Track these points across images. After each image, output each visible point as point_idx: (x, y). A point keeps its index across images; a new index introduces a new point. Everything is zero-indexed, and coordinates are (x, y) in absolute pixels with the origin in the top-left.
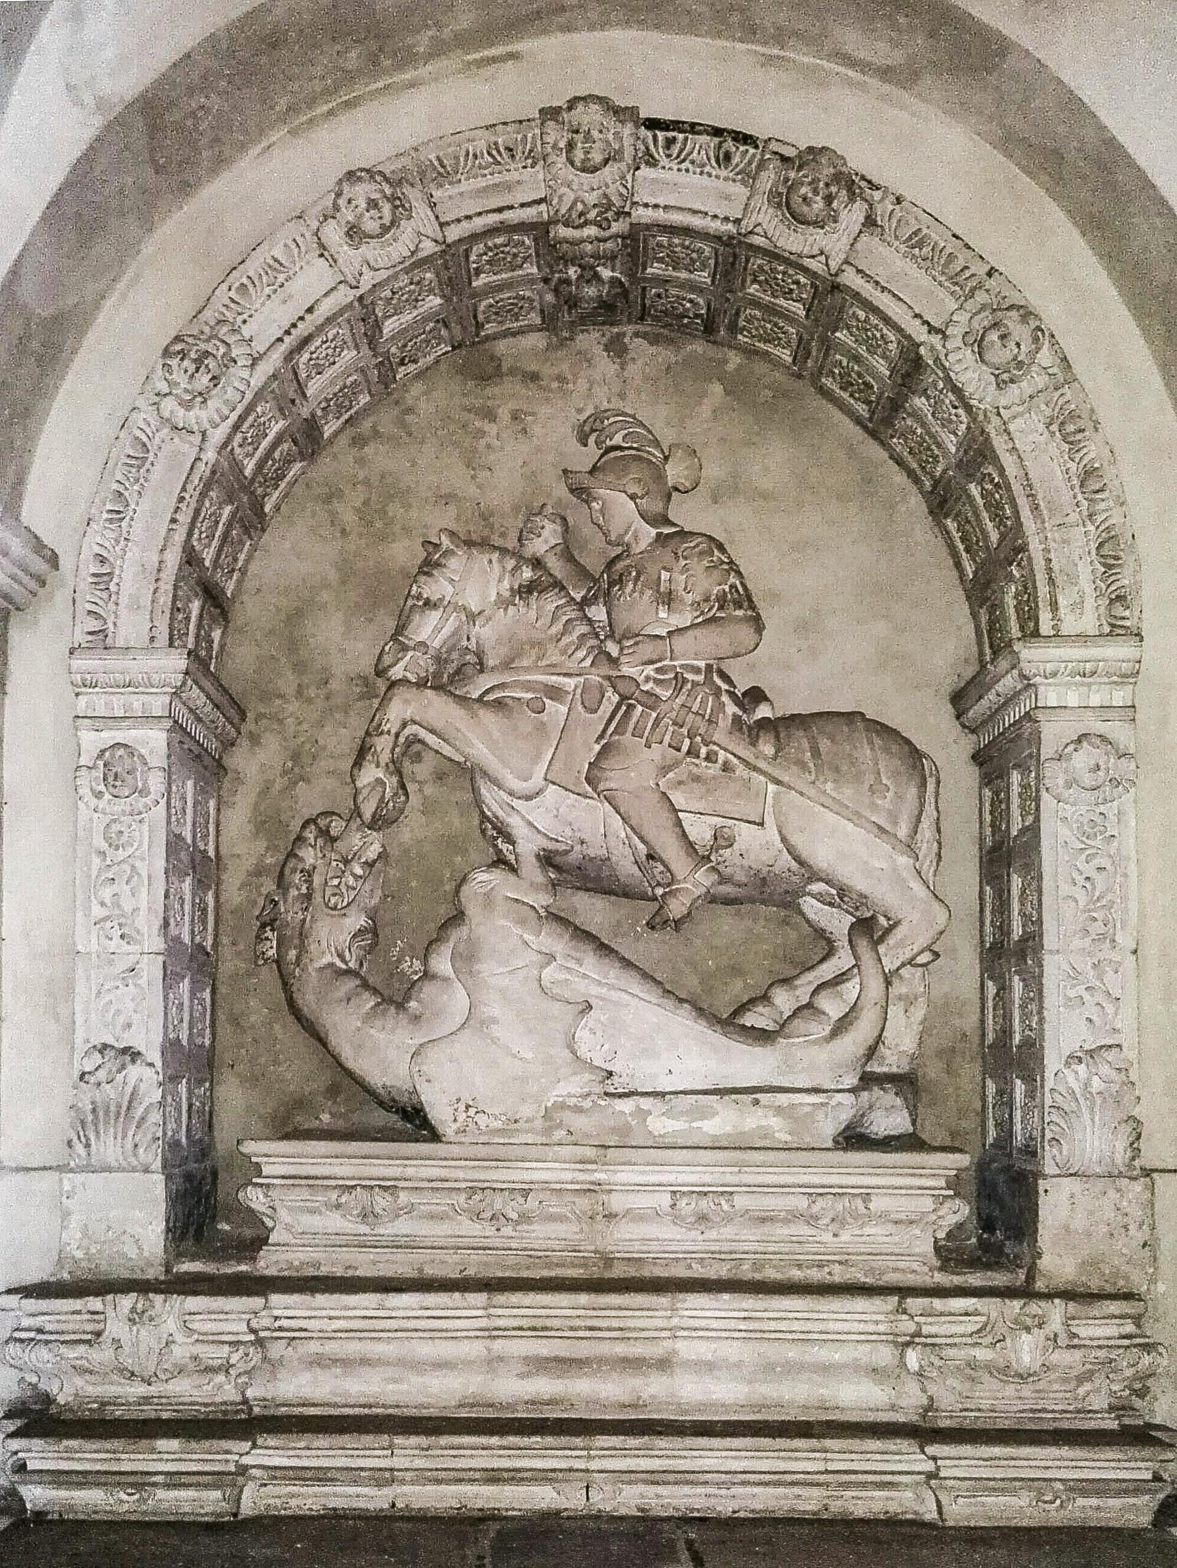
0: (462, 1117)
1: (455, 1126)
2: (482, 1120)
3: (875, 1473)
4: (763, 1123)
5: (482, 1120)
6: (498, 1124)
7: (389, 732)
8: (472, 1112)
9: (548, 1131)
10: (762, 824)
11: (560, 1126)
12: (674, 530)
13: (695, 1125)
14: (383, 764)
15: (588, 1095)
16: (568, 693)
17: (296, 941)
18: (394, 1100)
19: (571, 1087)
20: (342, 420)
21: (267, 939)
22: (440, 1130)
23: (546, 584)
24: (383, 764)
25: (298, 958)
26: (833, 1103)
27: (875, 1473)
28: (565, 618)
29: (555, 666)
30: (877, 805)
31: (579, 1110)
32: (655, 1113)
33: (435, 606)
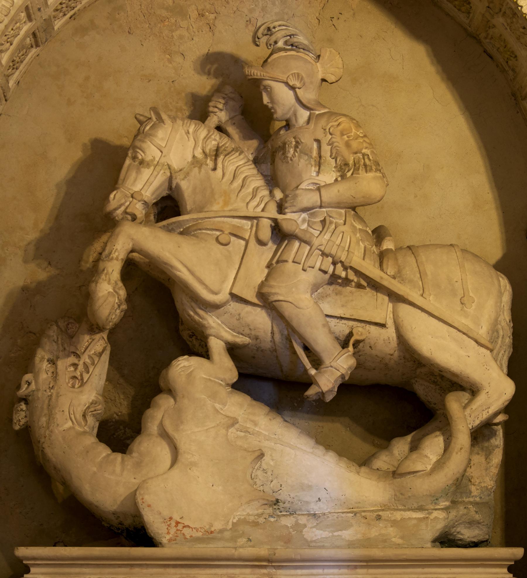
0: (173, 530)
1: (168, 537)
2: (186, 531)
3: (430, 573)
4: (383, 532)
5: (186, 531)
6: (200, 534)
7: (117, 259)
8: (180, 527)
9: (234, 539)
10: (383, 326)
11: (241, 536)
12: (326, 110)
13: (336, 534)
14: (112, 282)
15: (262, 514)
16: (246, 230)
17: (46, 411)
18: (121, 523)
19: (250, 511)
20: (69, 15)
21: (22, 410)
22: (157, 538)
23: (229, 149)
24: (112, 282)
25: (48, 423)
26: (432, 516)
27: (430, 573)
28: (243, 176)
29: (235, 210)
30: (359, 243)
31: (256, 524)
32: (309, 525)
33: (148, 165)
